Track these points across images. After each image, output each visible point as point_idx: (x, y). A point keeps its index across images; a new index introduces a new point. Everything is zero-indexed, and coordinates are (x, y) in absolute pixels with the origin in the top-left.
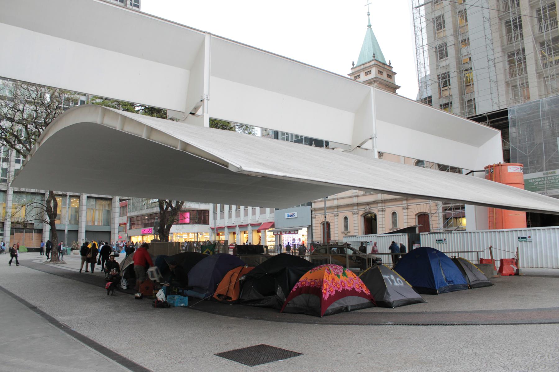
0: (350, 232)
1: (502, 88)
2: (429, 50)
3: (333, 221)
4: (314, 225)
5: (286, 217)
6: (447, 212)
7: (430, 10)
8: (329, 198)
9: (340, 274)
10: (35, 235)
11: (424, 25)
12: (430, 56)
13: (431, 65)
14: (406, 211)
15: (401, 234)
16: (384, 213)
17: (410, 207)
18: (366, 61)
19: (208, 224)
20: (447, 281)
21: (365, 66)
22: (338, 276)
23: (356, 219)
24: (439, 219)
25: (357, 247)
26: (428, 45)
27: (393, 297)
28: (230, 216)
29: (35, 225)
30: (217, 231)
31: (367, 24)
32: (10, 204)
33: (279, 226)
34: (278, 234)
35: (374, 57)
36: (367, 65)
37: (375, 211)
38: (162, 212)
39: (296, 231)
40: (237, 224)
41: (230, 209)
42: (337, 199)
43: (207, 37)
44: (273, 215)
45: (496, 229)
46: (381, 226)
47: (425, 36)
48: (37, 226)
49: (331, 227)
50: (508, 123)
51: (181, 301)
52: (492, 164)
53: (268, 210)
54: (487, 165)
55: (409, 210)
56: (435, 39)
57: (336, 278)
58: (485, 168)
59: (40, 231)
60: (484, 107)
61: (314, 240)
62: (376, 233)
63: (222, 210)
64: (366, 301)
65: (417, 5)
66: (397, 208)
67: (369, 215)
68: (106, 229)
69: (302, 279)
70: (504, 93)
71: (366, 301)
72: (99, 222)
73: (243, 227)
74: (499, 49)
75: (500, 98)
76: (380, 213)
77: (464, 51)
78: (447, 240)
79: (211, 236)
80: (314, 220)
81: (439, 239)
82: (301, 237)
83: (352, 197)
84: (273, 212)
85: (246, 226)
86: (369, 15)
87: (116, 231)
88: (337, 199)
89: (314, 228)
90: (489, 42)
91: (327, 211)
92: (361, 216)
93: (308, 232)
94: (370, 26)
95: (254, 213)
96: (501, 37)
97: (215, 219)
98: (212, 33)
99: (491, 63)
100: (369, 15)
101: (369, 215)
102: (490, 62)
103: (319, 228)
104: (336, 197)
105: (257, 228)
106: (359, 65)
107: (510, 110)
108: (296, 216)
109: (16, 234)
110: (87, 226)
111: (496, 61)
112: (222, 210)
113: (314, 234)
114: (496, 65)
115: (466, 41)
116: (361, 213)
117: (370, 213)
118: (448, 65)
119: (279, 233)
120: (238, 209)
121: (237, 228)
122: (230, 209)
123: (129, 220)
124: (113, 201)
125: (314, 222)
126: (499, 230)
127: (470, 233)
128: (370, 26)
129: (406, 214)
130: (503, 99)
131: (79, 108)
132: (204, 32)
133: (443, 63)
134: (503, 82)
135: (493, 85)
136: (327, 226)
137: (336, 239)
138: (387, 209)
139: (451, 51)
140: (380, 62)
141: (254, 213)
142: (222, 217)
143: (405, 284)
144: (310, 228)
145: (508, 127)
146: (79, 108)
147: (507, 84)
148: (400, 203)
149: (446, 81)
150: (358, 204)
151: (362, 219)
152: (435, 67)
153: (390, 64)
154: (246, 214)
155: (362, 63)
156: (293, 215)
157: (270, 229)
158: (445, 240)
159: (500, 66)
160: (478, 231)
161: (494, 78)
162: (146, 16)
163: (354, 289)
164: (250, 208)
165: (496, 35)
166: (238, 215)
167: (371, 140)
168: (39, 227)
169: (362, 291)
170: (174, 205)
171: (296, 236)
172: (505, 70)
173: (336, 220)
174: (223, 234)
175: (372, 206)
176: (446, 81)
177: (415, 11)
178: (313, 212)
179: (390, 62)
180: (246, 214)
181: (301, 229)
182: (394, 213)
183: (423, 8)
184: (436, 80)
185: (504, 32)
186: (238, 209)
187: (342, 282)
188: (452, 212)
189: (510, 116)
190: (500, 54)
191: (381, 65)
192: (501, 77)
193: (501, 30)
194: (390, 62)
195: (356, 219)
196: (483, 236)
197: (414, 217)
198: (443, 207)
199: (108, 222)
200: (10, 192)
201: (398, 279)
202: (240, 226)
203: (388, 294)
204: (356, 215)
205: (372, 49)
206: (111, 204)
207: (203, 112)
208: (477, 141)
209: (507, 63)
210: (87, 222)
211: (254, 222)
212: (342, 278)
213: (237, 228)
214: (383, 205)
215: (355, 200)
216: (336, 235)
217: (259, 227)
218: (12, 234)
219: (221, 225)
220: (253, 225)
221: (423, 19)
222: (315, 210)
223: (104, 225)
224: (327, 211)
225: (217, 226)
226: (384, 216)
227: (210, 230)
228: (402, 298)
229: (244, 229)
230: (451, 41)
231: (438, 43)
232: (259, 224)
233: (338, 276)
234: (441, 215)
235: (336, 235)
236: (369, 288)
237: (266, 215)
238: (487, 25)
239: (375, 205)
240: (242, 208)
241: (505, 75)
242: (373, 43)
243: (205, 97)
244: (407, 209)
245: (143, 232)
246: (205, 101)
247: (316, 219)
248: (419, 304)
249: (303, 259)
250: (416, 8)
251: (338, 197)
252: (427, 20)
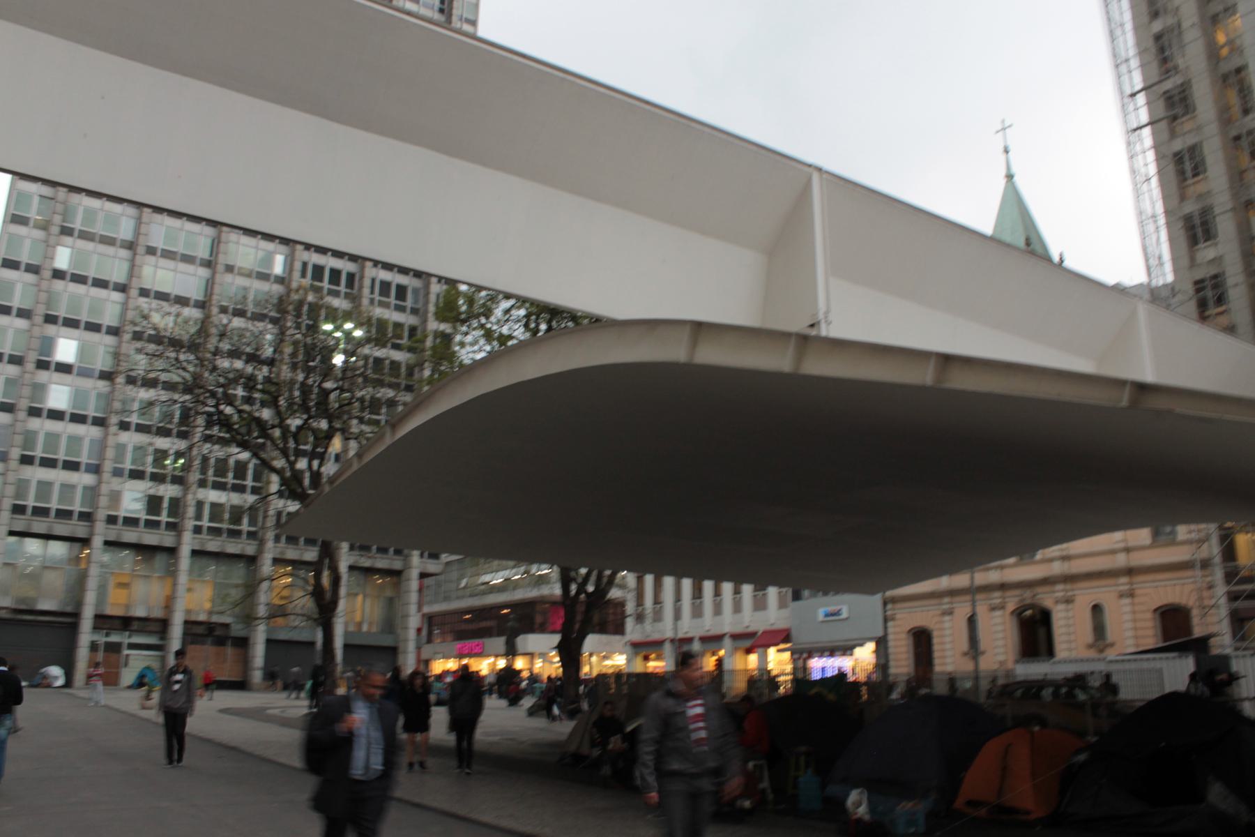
2: (1168, 224)
4: (890, 637)
5: (821, 617)
6: (1239, 604)
8: (1039, 555)
10: (230, 651)
12: (1172, 240)
13: (1175, 260)
14: (1127, 601)
16: (1070, 606)
17: (1138, 592)
23: (999, 620)
25: (1096, 682)
26: (1167, 212)
28: (718, 610)
31: (1003, 172)
33: (804, 637)
34: (801, 655)
37: (1048, 602)
39: (847, 650)
41: (717, 593)
42: (1065, 558)
44: (785, 613)
46: (1064, 638)
48: (237, 630)
55: (1137, 600)
56: (1183, 198)
59: (243, 643)
63: (698, 593)
65: (1135, 126)
68: (387, 641)
76: (1061, 607)
79: (629, 661)
83: (1113, 552)
86: (1006, 151)
87: (411, 646)
88: (1065, 558)
89: (891, 644)
92: (1012, 613)
94: (1010, 177)
95: (760, 605)
100: (1006, 151)
103: (903, 643)
104: (1057, 554)
105: (748, 643)
108: (844, 615)
112: (698, 593)
116: (1011, 606)
122: (717, 593)
125: (890, 630)
128: (1010, 177)
129: (1128, 609)
131: (542, 339)
132: (810, 166)
133: (1207, 253)
136: (922, 640)
137: (949, 668)
139: (1226, 226)
141: (760, 605)
142: (697, 612)
144: (882, 644)
146: (542, 339)
150: (1003, 587)
152: (1185, 262)
153: (1062, 261)
156: (837, 613)
157: (782, 646)
168: (242, 634)
171: (844, 663)
173: (947, 625)
174: (658, 658)
175: (1039, 590)
181: (861, 645)
182: (1097, 609)
195: (999, 620)
197: (1149, 615)
199: (391, 623)
204: (998, 613)
211: (738, 629)
214: (1068, 586)
215: (1121, 560)
216: (949, 660)
221: (1151, 156)
225: (680, 635)
226: (1070, 614)
229: (712, 646)
232: (752, 635)
235: (949, 660)
237: (774, 609)
251: (1072, 552)
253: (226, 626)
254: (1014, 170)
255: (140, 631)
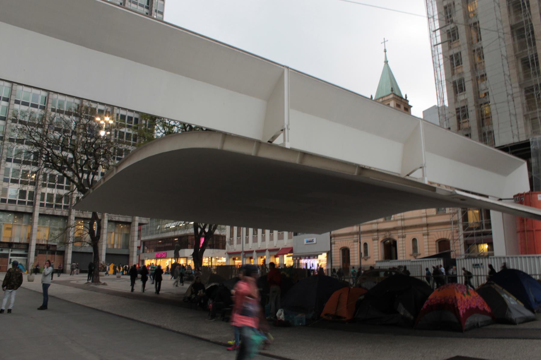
0: (420, 255)
1: (521, 122)
3: (352, 247)
4: (333, 251)
5: (305, 243)
6: (468, 239)
7: (447, 48)
9: (465, 293)
11: (442, 62)
14: (426, 237)
15: (436, 259)
17: (430, 233)
18: (384, 94)
19: (225, 249)
20: (535, 300)
21: (384, 99)
22: (464, 295)
24: (460, 246)
26: (447, 80)
27: (515, 315)
29: (58, 247)
30: (232, 255)
31: (384, 60)
32: (36, 226)
33: (298, 251)
34: (297, 258)
35: (392, 90)
36: (386, 98)
37: (395, 237)
38: (197, 236)
40: (254, 249)
41: (263, 233)
43: (286, 70)
45: (535, 253)
47: (443, 71)
49: (351, 252)
50: (530, 153)
51: (299, 317)
52: (522, 192)
53: (286, 234)
54: (516, 193)
55: (429, 237)
57: (463, 297)
58: (514, 196)
60: (505, 137)
61: (333, 265)
62: (396, 258)
64: (489, 318)
65: (435, 43)
66: (417, 234)
67: (388, 241)
68: (125, 252)
69: (431, 297)
70: (523, 125)
71: (489, 318)
72: (118, 245)
73: (261, 252)
74: (517, 85)
75: (520, 130)
76: (401, 239)
77: (482, 86)
78: (484, 264)
80: (333, 246)
81: (476, 263)
82: (320, 262)
84: (291, 238)
85: (264, 251)
86: (385, 51)
89: (333, 254)
90: (507, 78)
91: (361, 235)
92: (381, 242)
93: (327, 257)
94: (386, 62)
96: (518, 74)
97: (231, 243)
98: (291, 66)
99: (510, 97)
100: (385, 51)
101: (388, 241)
102: (510, 97)
105: (275, 253)
106: (377, 98)
107: (532, 142)
108: (315, 242)
109: (38, 255)
110: (107, 248)
111: (514, 95)
113: (333, 259)
114: (515, 99)
115: (483, 77)
116: (381, 239)
117: (389, 239)
118: (466, 99)
119: (298, 258)
120: (255, 233)
121: (255, 253)
123: (142, 243)
124: (132, 225)
125: (333, 248)
126: (538, 255)
127: (497, 258)
128: (386, 62)
130: (522, 130)
132: (283, 66)
133: (461, 97)
134: (522, 115)
135: (513, 118)
136: (346, 252)
138: (407, 236)
139: (469, 86)
140: (398, 96)
143: (518, 303)
145: (531, 157)
147: (526, 117)
148: (420, 229)
149: (465, 115)
150: (378, 231)
151: (382, 244)
152: (453, 100)
153: (406, 97)
154: (271, 238)
155: (380, 96)
156: (312, 241)
157: (289, 254)
158: (482, 264)
159: (518, 100)
160: (508, 256)
161: (513, 112)
162: (241, 52)
163: (477, 307)
164: (275, 232)
165: (514, 72)
166: (255, 240)
167: (421, 170)
169: (484, 309)
170: (207, 230)
172: (523, 104)
175: (392, 232)
176: (465, 115)
177: (433, 49)
178: (333, 238)
179: (406, 95)
180: (271, 238)
181: (321, 254)
182: (414, 240)
183: (440, 46)
184: (455, 113)
185: (521, 69)
186: (255, 233)
187: (468, 300)
188: (475, 238)
189: (532, 147)
190: (518, 90)
191: (399, 98)
192: (520, 111)
193: (517, 66)
194: (406, 95)
196: (521, 261)
197: (434, 243)
198: (464, 234)
199: (127, 245)
200: (36, 214)
201: (511, 298)
202: (258, 252)
203: (510, 311)
204: (376, 241)
205: (390, 83)
206: (130, 227)
207: (284, 140)
208: (505, 171)
209: (524, 98)
210: (107, 245)
211: (272, 247)
212: (467, 297)
213: (255, 253)
214: (403, 231)
217: (279, 252)
218: (36, 255)
219: (263, 248)
220: (270, 250)
221: (441, 56)
222: (335, 236)
223: (123, 248)
224: (361, 235)
227: (227, 255)
228: (521, 316)
229: (261, 254)
230: (468, 76)
231: (456, 78)
232: (277, 250)
233: (464, 295)
234: (462, 242)
236: (490, 306)
237: (286, 240)
238: (505, 62)
239: (395, 232)
240: (260, 231)
241: (523, 108)
242: (390, 78)
243: (286, 126)
244: (428, 235)
245: (157, 255)
246: (286, 130)
247: (335, 245)
248: (533, 322)
249: (344, 281)
250: (434, 46)
252: (445, 57)
253: (55, 246)
254: (388, 59)
255: (16, 249)
